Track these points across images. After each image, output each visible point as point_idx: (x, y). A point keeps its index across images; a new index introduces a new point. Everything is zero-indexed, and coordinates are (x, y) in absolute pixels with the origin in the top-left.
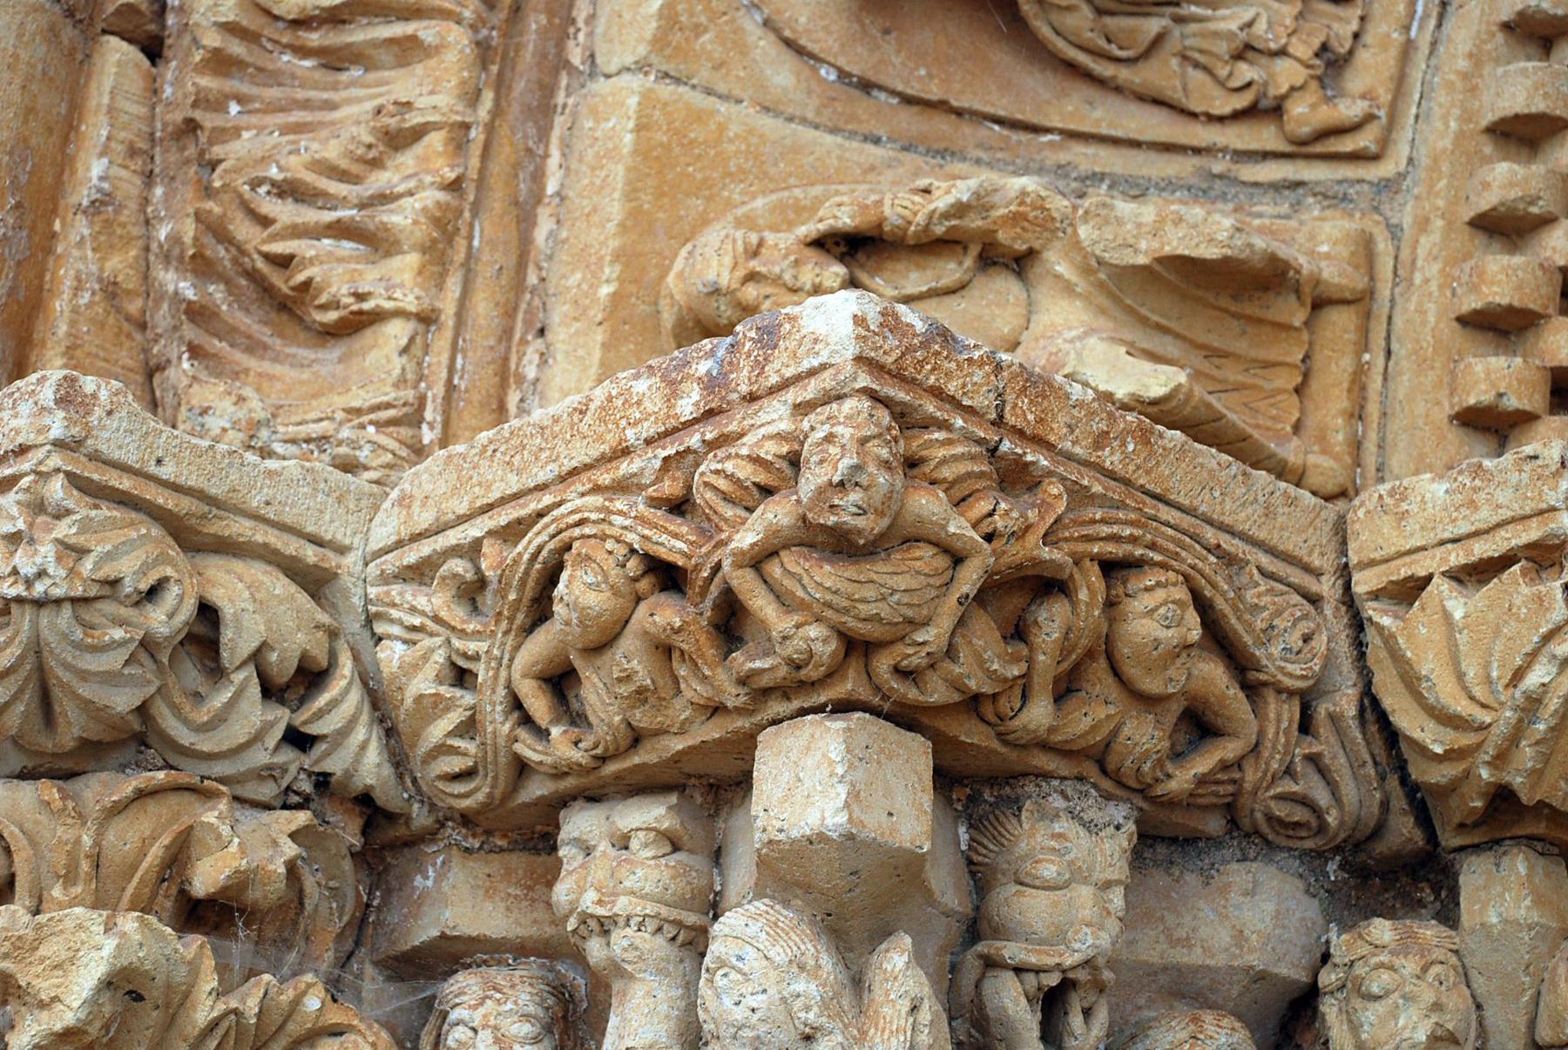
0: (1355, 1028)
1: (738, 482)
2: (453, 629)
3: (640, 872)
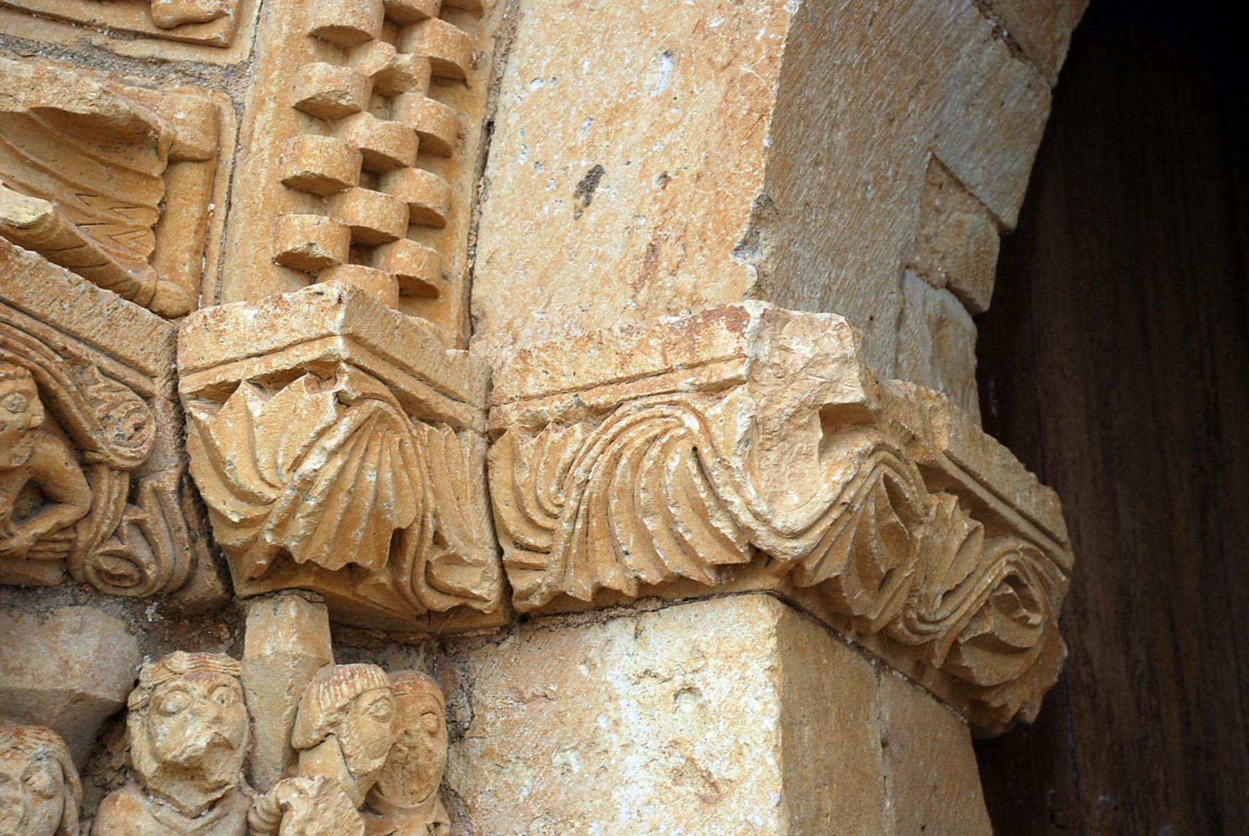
0: (152, 737)
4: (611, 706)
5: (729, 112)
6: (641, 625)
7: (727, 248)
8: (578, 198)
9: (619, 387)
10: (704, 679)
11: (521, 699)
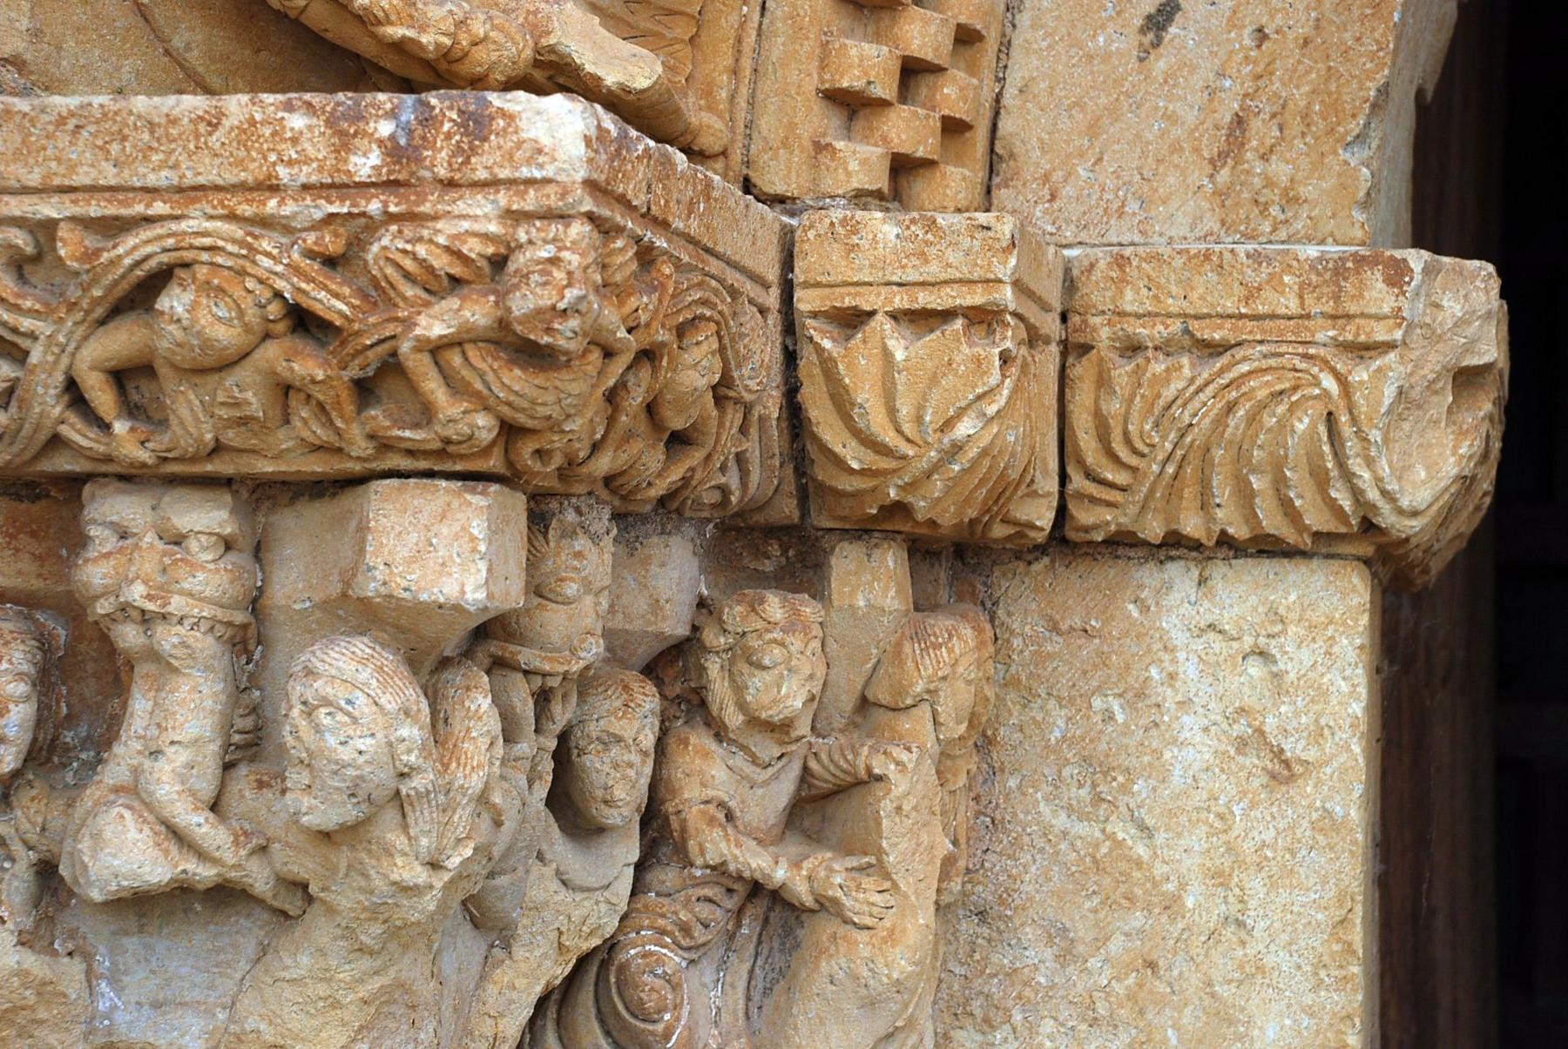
0: (739, 689)
1: (430, 270)
3: (201, 576)
4: (1167, 657)
6: (1206, 573)
7: (1338, 141)
8: (1145, 34)
9: (1240, 323)
10: (1282, 647)
11: (1055, 628)
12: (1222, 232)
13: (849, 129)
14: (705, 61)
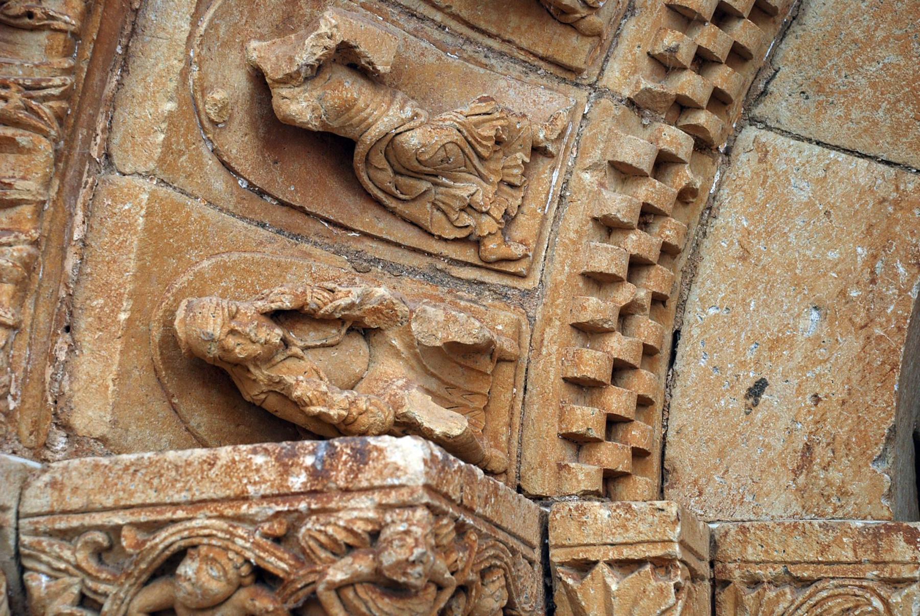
1: (335, 541)
2: (89, 575)
5: (867, 360)
9: (819, 567)
12: (804, 514)
13: (578, 456)
14: (493, 420)
